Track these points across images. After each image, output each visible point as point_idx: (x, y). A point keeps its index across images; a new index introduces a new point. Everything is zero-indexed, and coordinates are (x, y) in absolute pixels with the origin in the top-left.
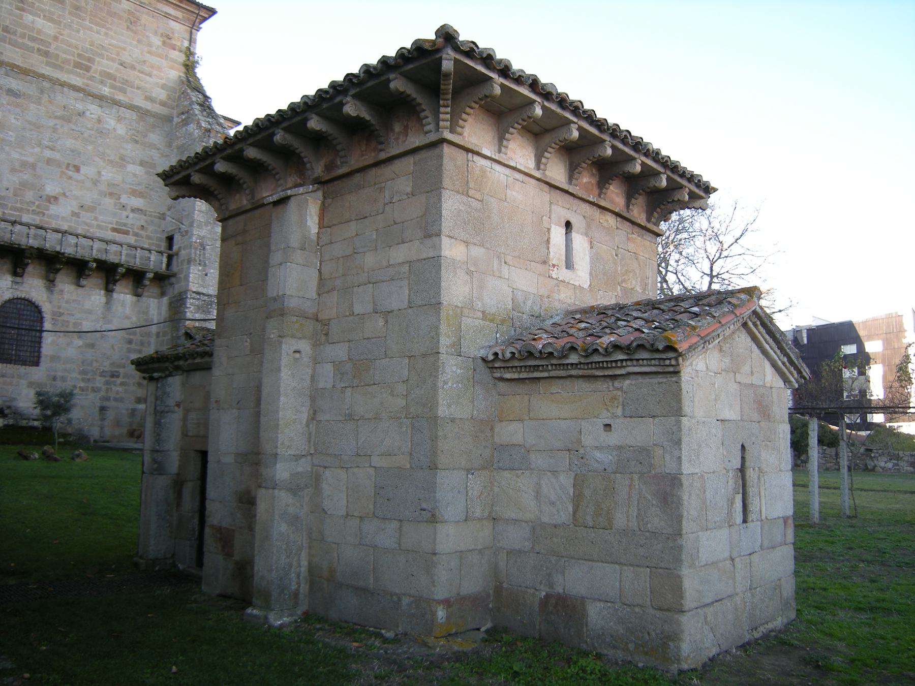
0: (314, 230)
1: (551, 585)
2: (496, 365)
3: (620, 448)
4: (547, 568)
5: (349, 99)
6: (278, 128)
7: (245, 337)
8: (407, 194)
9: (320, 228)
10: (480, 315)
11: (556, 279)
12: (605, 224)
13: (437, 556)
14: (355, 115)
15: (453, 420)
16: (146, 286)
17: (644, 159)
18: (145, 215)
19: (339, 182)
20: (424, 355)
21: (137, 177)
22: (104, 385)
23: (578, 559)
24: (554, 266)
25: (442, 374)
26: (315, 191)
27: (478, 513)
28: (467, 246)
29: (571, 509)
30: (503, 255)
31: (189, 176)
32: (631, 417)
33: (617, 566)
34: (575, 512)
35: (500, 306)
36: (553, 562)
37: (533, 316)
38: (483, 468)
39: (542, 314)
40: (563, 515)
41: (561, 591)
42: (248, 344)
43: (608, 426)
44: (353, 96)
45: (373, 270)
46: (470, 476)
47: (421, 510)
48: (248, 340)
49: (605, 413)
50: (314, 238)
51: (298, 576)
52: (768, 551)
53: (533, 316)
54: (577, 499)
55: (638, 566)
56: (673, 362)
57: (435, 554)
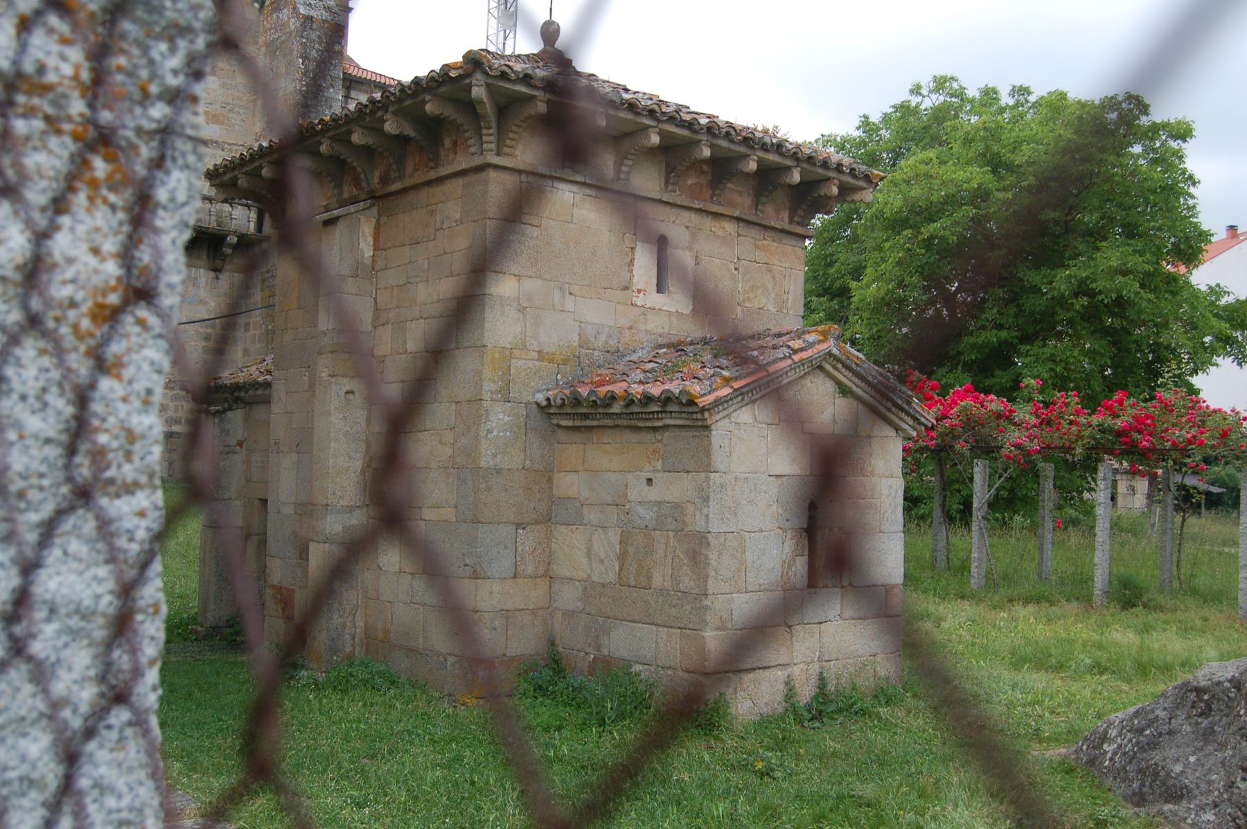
0: (368, 252)
1: (598, 648)
2: (552, 411)
3: (659, 504)
4: (595, 629)
5: (388, 116)
6: (324, 137)
7: (304, 369)
8: (456, 221)
9: (375, 250)
10: (536, 355)
11: (643, 306)
12: (720, 233)
13: (479, 614)
14: (398, 133)
15: (499, 471)
16: (227, 256)
17: (760, 154)
18: (223, 150)
19: (393, 198)
20: (469, 402)
21: (208, 93)
22: (172, 400)
23: (622, 620)
24: (639, 291)
25: (485, 422)
26: (369, 208)
27: (530, 570)
28: (519, 280)
29: (617, 568)
30: (567, 285)
31: (236, 178)
32: (669, 472)
33: (654, 627)
34: (621, 570)
35: (561, 343)
36: (601, 623)
37: (608, 352)
38: (537, 522)
39: (621, 349)
40: (611, 577)
41: (606, 654)
42: (306, 378)
43: (649, 480)
44: (394, 113)
45: (425, 304)
46: (520, 531)
47: (465, 565)
48: (307, 374)
49: (647, 467)
50: (368, 262)
51: (353, 638)
52: (854, 622)
53: (608, 352)
54: (623, 557)
55: (671, 627)
56: (699, 416)
57: (477, 611)
